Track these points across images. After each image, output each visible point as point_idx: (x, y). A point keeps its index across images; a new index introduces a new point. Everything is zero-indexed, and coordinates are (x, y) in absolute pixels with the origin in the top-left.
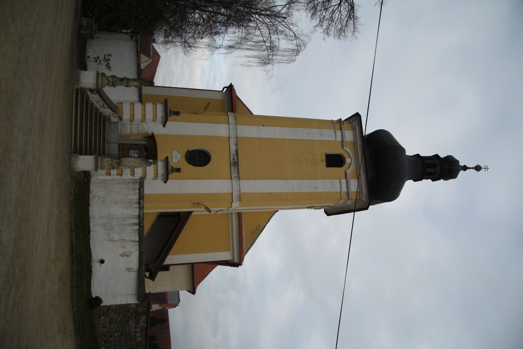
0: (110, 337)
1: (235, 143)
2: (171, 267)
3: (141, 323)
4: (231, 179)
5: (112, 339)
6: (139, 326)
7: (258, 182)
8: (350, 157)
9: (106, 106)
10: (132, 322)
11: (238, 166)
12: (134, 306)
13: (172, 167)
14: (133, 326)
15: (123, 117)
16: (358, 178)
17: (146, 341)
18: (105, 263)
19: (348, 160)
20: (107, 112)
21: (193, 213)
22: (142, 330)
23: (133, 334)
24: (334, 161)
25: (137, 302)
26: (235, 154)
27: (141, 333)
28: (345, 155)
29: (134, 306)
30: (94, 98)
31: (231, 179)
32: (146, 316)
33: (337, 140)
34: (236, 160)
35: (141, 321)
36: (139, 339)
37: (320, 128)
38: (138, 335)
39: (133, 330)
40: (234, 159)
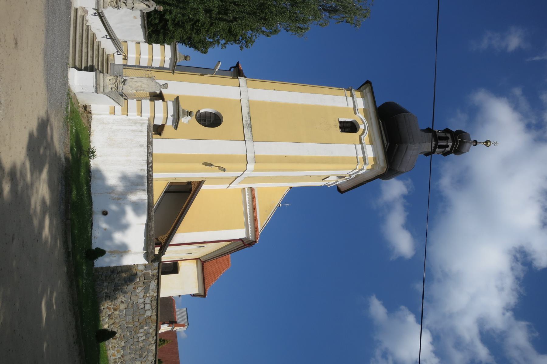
0: (115, 310)
1: (247, 105)
2: (179, 262)
3: (150, 291)
4: (245, 140)
5: (117, 313)
6: (148, 295)
7: (272, 144)
8: (364, 123)
9: (108, 37)
10: (140, 289)
11: (251, 127)
12: (142, 268)
13: (183, 110)
14: (142, 295)
15: (128, 55)
16: (371, 143)
17: (157, 315)
18: (107, 216)
19: (362, 127)
20: (108, 46)
21: (204, 187)
22: (151, 301)
23: (142, 306)
24: (349, 127)
25: (146, 263)
26: (247, 116)
27: (151, 304)
28: (360, 122)
29: (142, 268)
30: (95, 24)
31: (245, 140)
32: (157, 281)
33: (349, 106)
34: (249, 122)
35: (151, 287)
36: (148, 313)
37: (333, 158)
38: (148, 307)
39: (141, 301)
40: (246, 121)
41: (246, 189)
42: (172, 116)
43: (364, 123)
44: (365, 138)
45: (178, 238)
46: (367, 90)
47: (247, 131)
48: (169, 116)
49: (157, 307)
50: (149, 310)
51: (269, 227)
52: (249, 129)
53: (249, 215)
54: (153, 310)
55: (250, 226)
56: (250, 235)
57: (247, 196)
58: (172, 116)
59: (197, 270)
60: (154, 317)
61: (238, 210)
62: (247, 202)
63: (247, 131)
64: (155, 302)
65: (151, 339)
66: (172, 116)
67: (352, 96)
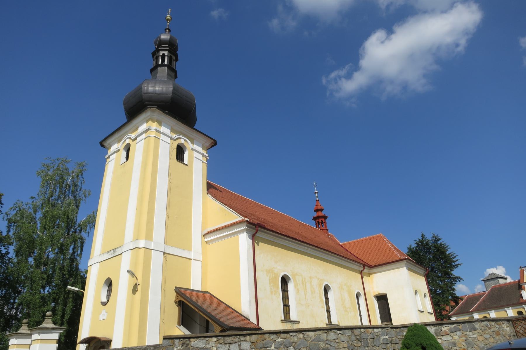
1: (102, 255)
22: (226, 344)
27: (231, 344)
32: (192, 340)
41: (206, 240)
42: (39, 335)
43: (125, 140)
44: (133, 136)
45: (246, 308)
46: (106, 144)
47: (118, 252)
48: (39, 338)
49: (236, 335)
50: (240, 346)
51: (239, 212)
52: (117, 250)
53: (227, 233)
54: (240, 341)
55: (236, 230)
56: (242, 228)
57: (212, 238)
58: (39, 335)
59: (381, 272)
60: (254, 338)
61: (220, 246)
62: (220, 235)
63: (118, 252)
64: (227, 338)
65: (295, 339)
66: (39, 334)
67: (109, 157)
